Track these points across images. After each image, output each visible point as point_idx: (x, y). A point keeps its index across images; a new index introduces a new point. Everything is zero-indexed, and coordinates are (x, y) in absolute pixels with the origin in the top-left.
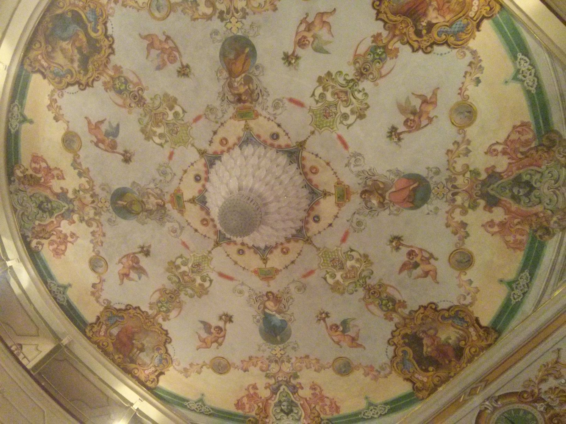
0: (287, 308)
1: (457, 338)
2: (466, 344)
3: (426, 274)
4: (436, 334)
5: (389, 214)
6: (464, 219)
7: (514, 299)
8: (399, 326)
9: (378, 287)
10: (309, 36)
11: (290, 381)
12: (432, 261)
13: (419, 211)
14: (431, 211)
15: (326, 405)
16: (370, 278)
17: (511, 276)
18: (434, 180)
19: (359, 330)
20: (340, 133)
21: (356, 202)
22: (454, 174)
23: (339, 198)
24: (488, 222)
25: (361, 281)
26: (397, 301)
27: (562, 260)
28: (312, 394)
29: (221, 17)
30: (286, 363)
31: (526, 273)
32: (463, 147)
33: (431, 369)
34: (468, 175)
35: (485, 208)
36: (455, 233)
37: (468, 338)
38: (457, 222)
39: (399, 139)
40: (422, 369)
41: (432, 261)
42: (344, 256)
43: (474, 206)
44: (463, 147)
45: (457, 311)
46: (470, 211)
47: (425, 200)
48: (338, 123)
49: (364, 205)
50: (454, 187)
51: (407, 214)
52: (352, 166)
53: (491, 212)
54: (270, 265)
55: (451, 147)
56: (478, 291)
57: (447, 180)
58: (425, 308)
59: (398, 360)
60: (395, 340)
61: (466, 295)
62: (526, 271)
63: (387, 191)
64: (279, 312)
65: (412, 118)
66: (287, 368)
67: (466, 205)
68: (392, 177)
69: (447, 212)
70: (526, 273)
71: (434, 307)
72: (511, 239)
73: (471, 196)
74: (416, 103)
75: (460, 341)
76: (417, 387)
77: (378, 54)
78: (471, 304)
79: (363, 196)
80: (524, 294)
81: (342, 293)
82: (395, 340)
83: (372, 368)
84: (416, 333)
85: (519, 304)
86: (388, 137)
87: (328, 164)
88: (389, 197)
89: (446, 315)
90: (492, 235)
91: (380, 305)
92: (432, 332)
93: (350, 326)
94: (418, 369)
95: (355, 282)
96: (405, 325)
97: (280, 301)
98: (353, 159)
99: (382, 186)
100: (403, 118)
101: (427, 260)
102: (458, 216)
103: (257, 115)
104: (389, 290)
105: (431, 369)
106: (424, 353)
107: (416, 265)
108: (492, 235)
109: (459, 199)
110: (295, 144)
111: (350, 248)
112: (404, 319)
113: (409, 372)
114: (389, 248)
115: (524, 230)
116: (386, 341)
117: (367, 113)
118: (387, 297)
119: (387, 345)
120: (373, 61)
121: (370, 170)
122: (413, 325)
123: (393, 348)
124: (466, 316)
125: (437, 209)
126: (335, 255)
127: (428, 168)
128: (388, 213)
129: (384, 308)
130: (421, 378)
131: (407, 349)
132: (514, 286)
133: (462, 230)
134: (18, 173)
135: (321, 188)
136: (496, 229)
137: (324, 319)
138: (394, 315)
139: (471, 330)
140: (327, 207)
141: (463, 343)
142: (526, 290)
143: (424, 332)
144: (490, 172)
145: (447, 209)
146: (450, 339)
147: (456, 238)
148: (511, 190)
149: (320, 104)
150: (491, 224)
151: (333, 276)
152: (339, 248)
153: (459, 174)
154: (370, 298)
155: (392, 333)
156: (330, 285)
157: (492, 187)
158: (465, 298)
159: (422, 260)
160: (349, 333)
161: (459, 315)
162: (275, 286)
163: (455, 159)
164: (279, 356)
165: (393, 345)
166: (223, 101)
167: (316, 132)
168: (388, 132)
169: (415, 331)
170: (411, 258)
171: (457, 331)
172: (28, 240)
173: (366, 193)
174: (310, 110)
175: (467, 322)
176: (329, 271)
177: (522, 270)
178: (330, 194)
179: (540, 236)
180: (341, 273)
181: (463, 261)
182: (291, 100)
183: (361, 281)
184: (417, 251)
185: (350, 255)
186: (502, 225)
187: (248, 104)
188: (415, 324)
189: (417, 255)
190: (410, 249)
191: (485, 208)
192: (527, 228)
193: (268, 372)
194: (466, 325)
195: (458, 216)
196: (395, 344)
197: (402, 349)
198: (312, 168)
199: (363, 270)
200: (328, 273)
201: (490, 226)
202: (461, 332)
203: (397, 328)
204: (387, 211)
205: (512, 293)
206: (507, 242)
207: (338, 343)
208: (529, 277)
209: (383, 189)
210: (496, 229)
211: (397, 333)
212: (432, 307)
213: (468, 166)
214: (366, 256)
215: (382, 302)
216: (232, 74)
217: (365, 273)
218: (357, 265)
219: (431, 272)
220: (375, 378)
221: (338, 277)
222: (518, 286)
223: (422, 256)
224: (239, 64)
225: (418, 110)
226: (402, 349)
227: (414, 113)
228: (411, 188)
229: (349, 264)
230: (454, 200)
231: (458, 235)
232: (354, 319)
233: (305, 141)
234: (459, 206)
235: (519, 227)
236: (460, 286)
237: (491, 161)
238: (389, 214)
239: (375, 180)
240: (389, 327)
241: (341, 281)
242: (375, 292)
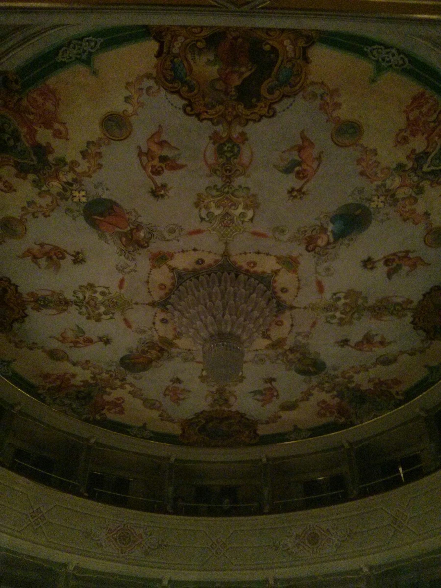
0: (314, 228)
1: (199, 55)
2: (197, 41)
3: (162, 144)
4: (218, 79)
5: (140, 216)
6: (79, 159)
7: (96, 43)
8: (243, 121)
9: (218, 173)
10: (81, 339)
11: (412, 168)
12: (145, 150)
13: (114, 199)
14: (103, 189)
15: (421, 112)
16: (215, 186)
17: (81, 68)
18: (77, 208)
19: (284, 152)
20: (117, 290)
21: (156, 246)
22: (56, 198)
23: (166, 260)
24: (60, 138)
25: (226, 190)
26: (217, 145)
27: (11, 40)
28: (414, 136)
29: (124, 379)
30: (387, 187)
31: (60, 58)
32: (31, 210)
33: (267, 48)
34: (44, 188)
35: (52, 152)
36: (99, 154)
37: (188, 45)
38: (89, 162)
39: (78, 253)
40: (277, 56)
41: (145, 150)
42: (213, 222)
43: (61, 161)
44: (31, 210)
45: (171, 82)
46: (68, 160)
47: (100, 202)
48: (112, 295)
49: (152, 239)
50: (65, 190)
51: (126, 205)
52: (131, 268)
53: (49, 144)
54: (277, 266)
55: (41, 217)
56: (128, 84)
57: (67, 199)
58: (198, 115)
59: (287, 89)
60: (264, 111)
61: (144, 92)
62: (59, 61)
63: (124, 232)
64: (324, 230)
65: (54, 257)
66: (394, 182)
67: (67, 168)
68: (109, 238)
69: (90, 177)
70: (60, 58)
71: (189, 109)
72: (49, 105)
73: (57, 171)
74: (43, 262)
75: (200, 50)
76: (306, 43)
77: (44, 302)
78: (148, 76)
79: (146, 245)
80: (81, 39)
81: (255, 196)
82: (264, 111)
83: (322, 108)
84: (235, 100)
85: (98, 34)
86: (85, 262)
87: (148, 282)
88: (127, 227)
89: (185, 89)
90: (65, 123)
91: (236, 155)
92: (220, 85)
93: (286, 163)
94: (280, 59)
95: (233, 194)
96: (237, 116)
97: (311, 237)
98: (125, 270)
99: (124, 239)
100: (62, 262)
101: (149, 154)
102: (83, 166)
103: (161, 337)
104: (211, 161)
105: (267, 48)
106: (253, 70)
107: (163, 159)
108: (65, 123)
109: (70, 177)
110: (157, 308)
111: (202, 221)
112: (230, 124)
113: (293, 65)
114: (171, 193)
115: (29, 102)
116: (274, 119)
117: (85, 284)
118: (221, 157)
119: (278, 114)
120: (51, 302)
121: (121, 255)
122: (230, 110)
123: (275, 106)
124: (166, 69)
125: (96, 187)
126: (220, 228)
127: (74, 219)
128: (139, 218)
129: (236, 149)
130: (290, 48)
131: (264, 92)
132: (85, 56)
133: (90, 151)
134: (343, 420)
135: (171, 275)
136: (57, 126)
137: (299, 190)
138: (235, 135)
139: (175, 50)
140: (182, 262)
141: (199, 44)
142: (74, 42)
143: (226, 93)
144: (23, 175)
145: (87, 179)
146: (209, 60)
147: (103, 149)
148: (15, 147)
149: (113, 311)
150: (57, 134)
151: (243, 215)
152: (210, 229)
153: (51, 195)
154: (237, 170)
155: (259, 121)
156: (254, 212)
157: (32, 163)
158: (150, 88)
159: (153, 159)
160: (297, 158)
161: (172, 76)
162: (297, 250)
163: (46, 207)
164: (382, 198)
165: (273, 109)
166: (172, 357)
167: (133, 302)
168: (82, 263)
169: (234, 103)
170: (160, 169)
171: (192, 63)
172: (398, 402)
173: (142, 245)
174: (123, 313)
175: (172, 61)
176: (240, 223)
177: (63, 65)
178: (169, 267)
179: (17, 83)
180: (232, 211)
181: (115, 125)
182: (129, 326)
183: (226, 190)
184: (150, 169)
185: (208, 217)
186: (48, 125)
187: (160, 345)
188: (226, 109)
189: (153, 167)
190: (154, 177)
191: (52, 152)
192: (25, 102)
193: (414, 194)
194: (176, 60)
195: (83, 166)
196: (270, 107)
197: (269, 97)
198: (161, 289)
199: (213, 197)
200: (243, 222)
201: (61, 133)
202: (190, 57)
203: (247, 121)
204: (139, 220)
205: (93, 51)
206: (57, 104)
207: (319, 159)
208: (61, 51)
209: (126, 236)
210: (57, 126)
211: (254, 116)
212: (190, 109)
213: (39, 194)
214: (197, 205)
215: (232, 156)
216: (150, 361)
217: (214, 192)
218: (213, 205)
219: (156, 140)
220: (335, 92)
221: (240, 210)
222: (80, 52)
223: (149, 161)
224: (141, 360)
225: (45, 257)
226: (269, 97)
227: (50, 258)
228: (102, 219)
229: (217, 212)
230: (75, 180)
231: (99, 151)
232: (276, 166)
233: (148, 304)
234: (75, 172)
235: (33, 110)
236: (142, 105)
237: (15, 181)
238: (140, 216)
239: (125, 246)
240: (252, 129)
241: (241, 207)
242: (226, 171)
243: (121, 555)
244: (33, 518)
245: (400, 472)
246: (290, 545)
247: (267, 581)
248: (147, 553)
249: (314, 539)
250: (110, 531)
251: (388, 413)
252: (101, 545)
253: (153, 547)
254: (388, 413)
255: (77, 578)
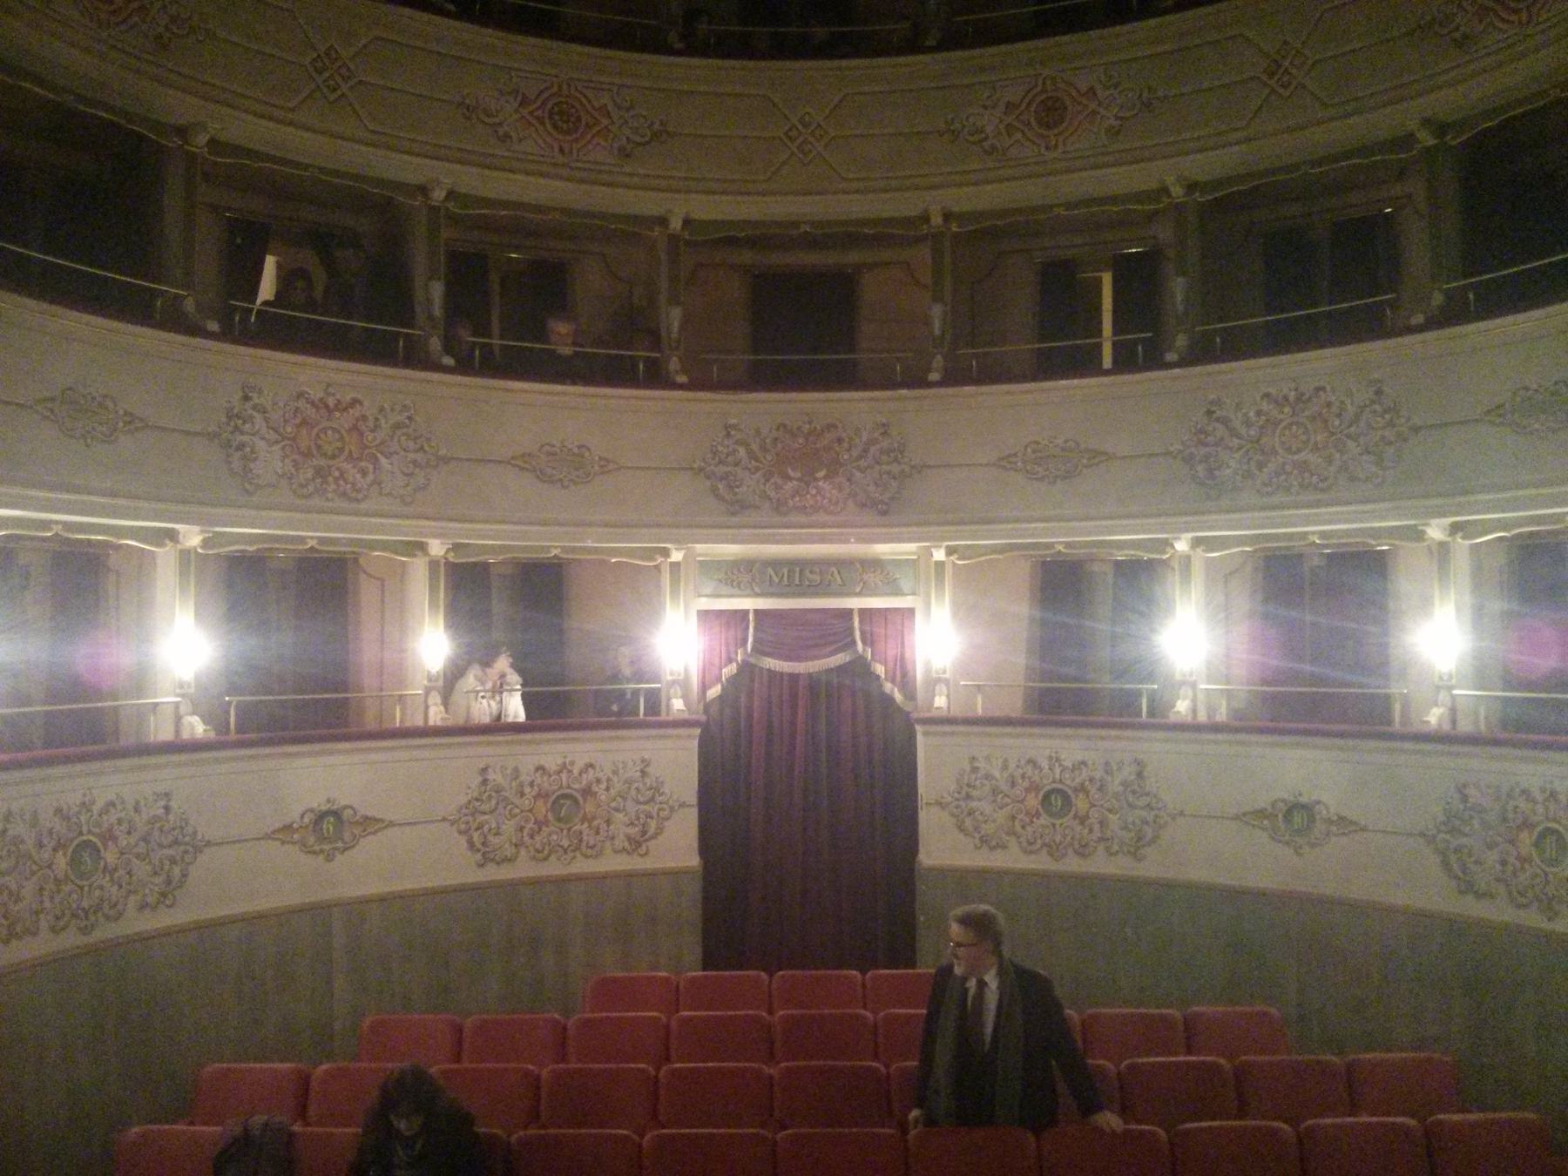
243: (561, 159)
244: (320, 73)
245: (1114, 344)
246: (989, 129)
247: (925, 218)
248: (625, 154)
249: (1052, 112)
250: (525, 102)
251: (1456, 1117)
252: (507, 136)
253: (638, 139)
254: (1456, 1117)
255: (454, 220)
